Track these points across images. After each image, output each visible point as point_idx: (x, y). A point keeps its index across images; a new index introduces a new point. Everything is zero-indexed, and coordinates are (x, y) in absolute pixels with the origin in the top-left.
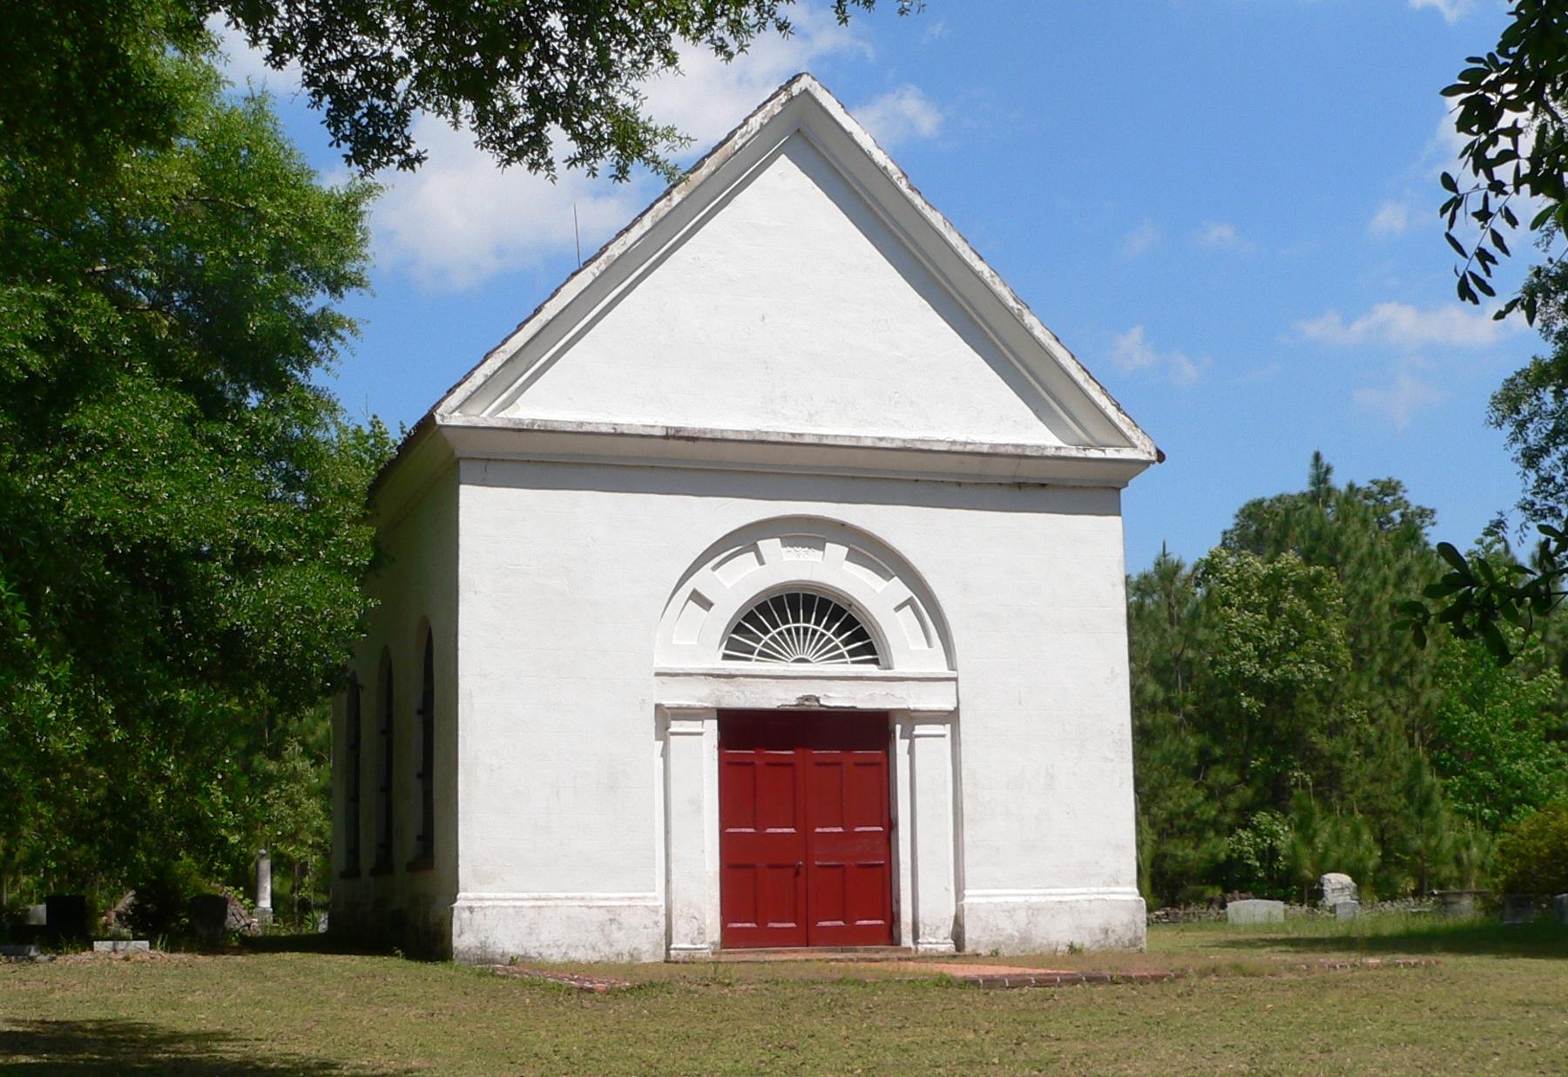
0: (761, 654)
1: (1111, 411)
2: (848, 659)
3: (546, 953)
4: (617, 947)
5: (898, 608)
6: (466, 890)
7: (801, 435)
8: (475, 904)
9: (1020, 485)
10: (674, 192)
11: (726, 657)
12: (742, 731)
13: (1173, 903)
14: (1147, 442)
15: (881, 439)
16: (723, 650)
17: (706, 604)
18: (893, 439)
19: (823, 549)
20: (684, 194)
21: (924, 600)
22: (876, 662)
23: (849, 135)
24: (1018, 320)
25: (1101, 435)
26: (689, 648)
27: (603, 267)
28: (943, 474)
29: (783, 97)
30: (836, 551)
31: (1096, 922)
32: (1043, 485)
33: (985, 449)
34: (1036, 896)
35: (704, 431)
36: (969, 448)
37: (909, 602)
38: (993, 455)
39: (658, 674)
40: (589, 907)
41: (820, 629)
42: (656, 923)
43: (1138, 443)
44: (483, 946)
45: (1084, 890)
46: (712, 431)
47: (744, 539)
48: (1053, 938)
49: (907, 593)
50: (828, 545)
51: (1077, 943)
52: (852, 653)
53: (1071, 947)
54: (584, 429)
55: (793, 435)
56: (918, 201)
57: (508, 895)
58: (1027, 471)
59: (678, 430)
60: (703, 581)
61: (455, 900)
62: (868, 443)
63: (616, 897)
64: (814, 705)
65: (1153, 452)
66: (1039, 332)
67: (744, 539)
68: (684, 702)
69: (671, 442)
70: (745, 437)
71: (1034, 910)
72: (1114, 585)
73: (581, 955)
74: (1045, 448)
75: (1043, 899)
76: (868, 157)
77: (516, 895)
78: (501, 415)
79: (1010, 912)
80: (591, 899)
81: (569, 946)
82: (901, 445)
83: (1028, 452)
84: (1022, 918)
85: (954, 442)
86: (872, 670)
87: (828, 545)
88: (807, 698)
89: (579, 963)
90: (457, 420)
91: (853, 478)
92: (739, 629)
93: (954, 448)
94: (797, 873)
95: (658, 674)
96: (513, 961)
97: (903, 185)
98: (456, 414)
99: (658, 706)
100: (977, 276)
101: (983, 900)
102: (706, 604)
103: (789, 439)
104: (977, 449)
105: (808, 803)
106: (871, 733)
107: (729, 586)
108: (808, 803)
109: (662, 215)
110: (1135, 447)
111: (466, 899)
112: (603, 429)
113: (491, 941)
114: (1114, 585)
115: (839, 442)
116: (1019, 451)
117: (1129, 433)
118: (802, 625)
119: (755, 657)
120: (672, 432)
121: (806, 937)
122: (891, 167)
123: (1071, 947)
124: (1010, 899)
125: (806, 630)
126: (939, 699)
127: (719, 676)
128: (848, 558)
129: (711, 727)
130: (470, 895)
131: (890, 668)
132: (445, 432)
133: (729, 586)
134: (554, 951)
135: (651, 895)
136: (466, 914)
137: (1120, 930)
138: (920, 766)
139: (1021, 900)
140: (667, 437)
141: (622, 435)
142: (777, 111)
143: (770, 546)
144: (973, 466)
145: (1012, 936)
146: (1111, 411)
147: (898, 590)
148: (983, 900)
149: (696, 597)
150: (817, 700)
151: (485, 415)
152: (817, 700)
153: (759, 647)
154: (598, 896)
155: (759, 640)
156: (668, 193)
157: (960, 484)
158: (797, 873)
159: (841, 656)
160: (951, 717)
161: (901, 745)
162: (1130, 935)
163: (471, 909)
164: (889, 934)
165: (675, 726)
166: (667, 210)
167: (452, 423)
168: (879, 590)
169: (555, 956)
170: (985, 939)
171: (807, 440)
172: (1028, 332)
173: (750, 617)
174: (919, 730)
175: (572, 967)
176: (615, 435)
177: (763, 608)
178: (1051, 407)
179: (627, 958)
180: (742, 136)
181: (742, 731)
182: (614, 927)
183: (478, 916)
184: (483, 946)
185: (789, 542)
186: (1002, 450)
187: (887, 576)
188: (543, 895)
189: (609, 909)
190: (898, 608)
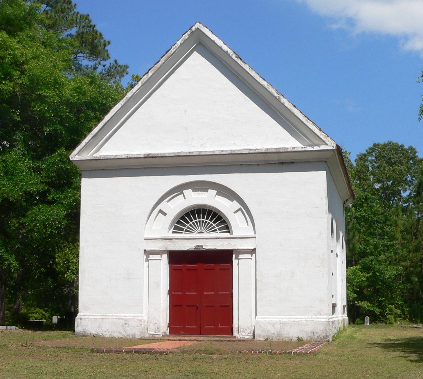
0: (186, 231)
1: (317, 132)
2: (218, 231)
3: (105, 334)
4: (128, 333)
5: (235, 212)
6: (81, 313)
7: (192, 152)
8: (82, 317)
9: (283, 163)
10: (150, 72)
11: (173, 232)
12: (176, 258)
13: (354, 323)
14: (333, 142)
15: (222, 151)
16: (172, 230)
17: (165, 214)
18: (227, 151)
19: (207, 192)
20: (153, 72)
21: (245, 208)
22: (229, 232)
23: (214, 42)
24: (279, 100)
25: (316, 141)
26: (160, 230)
27: (125, 101)
28: (197, 163)
29: (189, 32)
30: (212, 192)
31: (309, 329)
32: (293, 162)
33: (263, 151)
34: (285, 319)
35: (158, 154)
36: (257, 151)
37: (240, 209)
38: (267, 153)
39: (145, 239)
40: (118, 319)
41: (197, 220)
42: (141, 325)
43: (328, 143)
44: (84, 331)
45: (306, 317)
46: (160, 154)
47: (179, 190)
48: (291, 335)
49: (239, 206)
50: (209, 190)
51: (300, 336)
52: (220, 229)
53: (298, 339)
54: (117, 157)
55: (189, 152)
56: (239, 61)
57: (93, 314)
58: (283, 158)
59: (149, 155)
60: (162, 206)
61: (76, 316)
62: (218, 153)
63: (128, 315)
64: (201, 249)
65: (335, 145)
66: (287, 104)
67: (179, 190)
68: (153, 249)
69: (147, 159)
70: (172, 155)
71: (283, 324)
72: (322, 199)
73: (116, 335)
74: (288, 148)
75: (288, 320)
76: (221, 48)
77: (96, 314)
78: (95, 155)
79: (273, 324)
80: (120, 316)
81: (112, 332)
82: (230, 152)
83: (281, 151)
84: (278, 327)
85: (251, 150)
86: (227, 235)
87: (209, 190)
88: (199, 246)
89: (115, 338)
90: (77, 158)
91: (217, 166)
92: (179, 222)
93: (251, 152)
94: (197, 308)
95: (145, 239)
96: (94, 336)
97: (234, 57)
98: (77, 156)
99: (145, 250)
100: (262, 86)
101: (263, 320)
102: (165, 214)
103: (188, 154)
104: (260, 151)
105: (201, 284)
106: (225, 258)
107: (172, 207)
108: (201, 284)
109: (145, 80)
110: (327, 144)
111: (80, 315)
112: (124, 157)
113: (87, 329)
114: (322, 199)
115: (207, 154)
116: (277, 151)
117: (324, 139)
118: (208, 221)
119: (184, 232)
120: (146, 156)
121: (200, 331)
122: (229, 51)
123: (298, 339)
124: (273, 320)
125: (196, 222)
126: (248, 245)
127: (166, 239)
128: (217, 194)
129: (165, 257)
130: (82, 314)
131: (232, 234)
132: (74, 163)
133: (172, 207)
134: (107, 333)
135: (141, 315)
136: (79, 320)
137: (320, 333)
138: (242, 270)
139: (278, 320)
140: (145, 157)
141: (130, 158)
142: (186, 38)
143: (188, 192)
144: (261, 158)
145: (274, 334)
146: (317, 132)
147: (236, 205)
148: (263, 320)
149: (161, 211)
150: (202, 246)
151: (87, 156)
152: (202, 246)
153: (185, 228)
154: (123, 315)
155: (185, 226)
156: (147, 73)
157: (258, 165)
158: (197, 308)
159: (216, 230)
160: (253, 251)
161: (235, 262)
162: (324, 334)
163: (81, 319)
164: (230, 331)
165: (151, 257)
166: (147, 79)
167: (75, 159)
168: (228, 206)
169: (107, 335)
170: (263, 334)
171: (194, 154)
172: (283, 104)
173: (183, 218)
174: (241, 256)
175: (112, 340)
176: (127, 158)
177: (187, 215)
178: (296, 132)
179: (131, 337)
180: (174, 49)
181: (176, 258)
182: (127, 325)
183: (83, 321)
184: (84, 331)
185: (194, 190)
186: (270, 151)
187: (232, 200)
188: (105, 314)
189: (125, 320)
190: (235, 212)
